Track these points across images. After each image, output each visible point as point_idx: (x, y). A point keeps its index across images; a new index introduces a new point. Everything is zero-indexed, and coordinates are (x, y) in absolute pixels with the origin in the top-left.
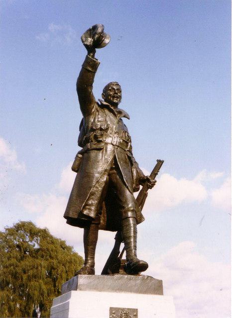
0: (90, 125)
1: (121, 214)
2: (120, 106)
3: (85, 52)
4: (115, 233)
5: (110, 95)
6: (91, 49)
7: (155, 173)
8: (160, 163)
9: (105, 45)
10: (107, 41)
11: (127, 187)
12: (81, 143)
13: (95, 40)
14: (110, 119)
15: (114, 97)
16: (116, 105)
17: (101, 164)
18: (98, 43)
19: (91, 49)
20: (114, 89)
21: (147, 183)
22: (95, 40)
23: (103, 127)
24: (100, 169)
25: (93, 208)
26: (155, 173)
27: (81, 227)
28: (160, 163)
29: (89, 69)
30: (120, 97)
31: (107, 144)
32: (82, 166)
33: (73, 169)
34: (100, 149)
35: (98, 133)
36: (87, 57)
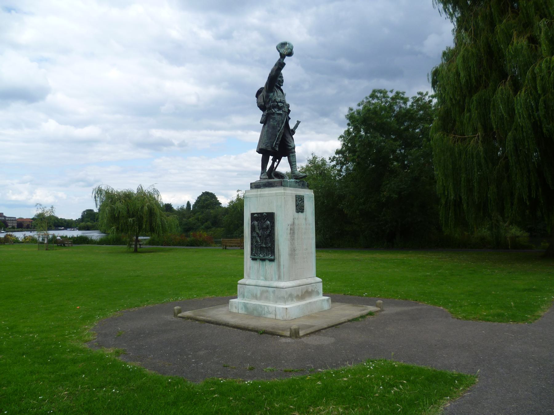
7: (296, 127)
8: (298, 122)
21: (293, 132)
26: (296, 127)
28: (298, 122)
29: (280, 65)
35: (279, 104)
36: (279, 60)
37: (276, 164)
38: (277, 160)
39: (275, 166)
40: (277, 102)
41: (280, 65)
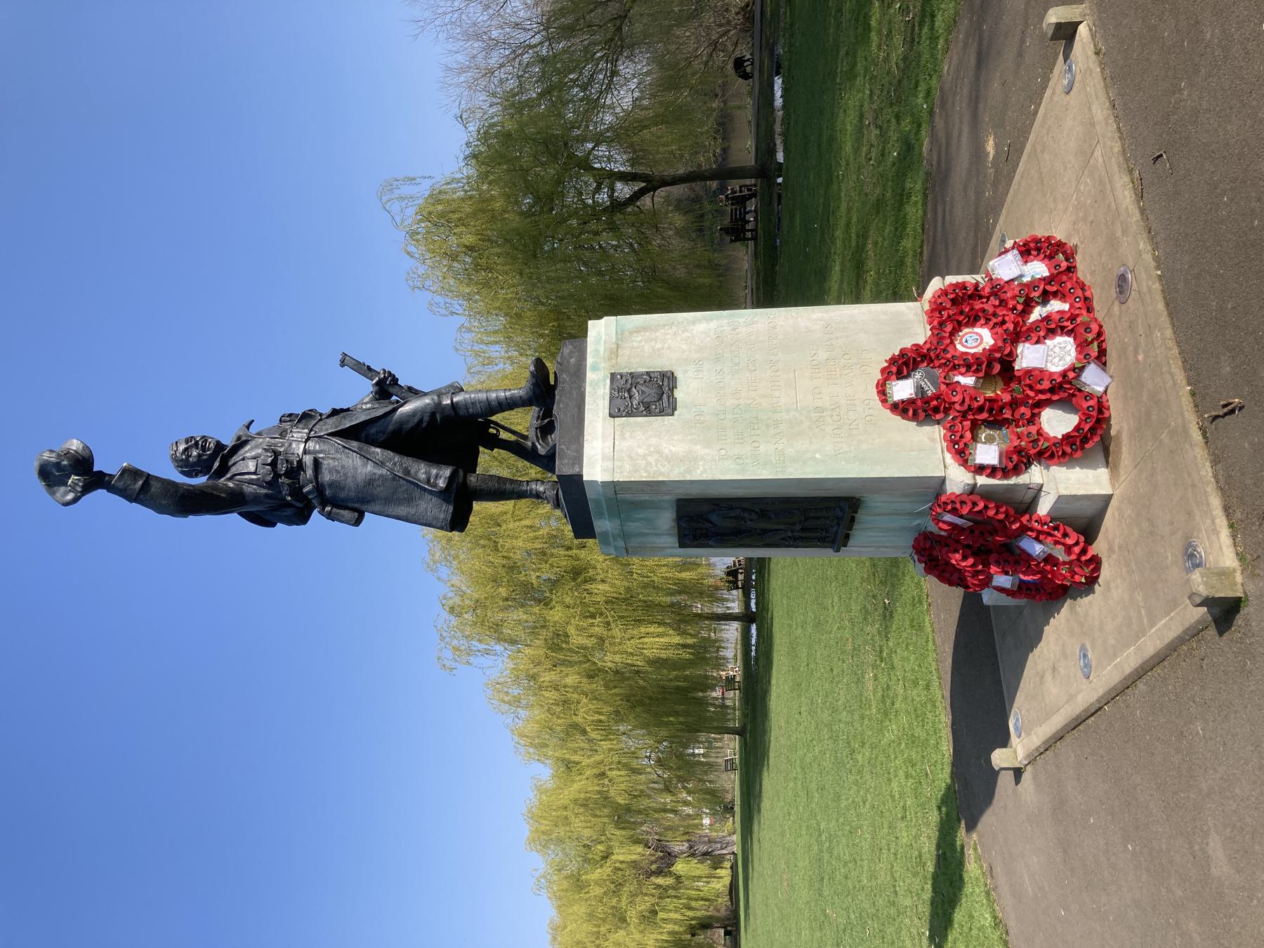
0: (264, 491)
1: (446, 419)
2: (229, 441)
3: (101, 494)
4: (481, 449)
5: (199, 455)
6: (95, 480)
7: (368, 371)
9: (86, 447)
10: (75, 445)
11: (395, 410)
12: (301, 517)
13: (78, 473)
14: (252, 449)
15: (204, 449)
16: (219, 446)
17: (352, 465)
18: (82, 464)
19: (95, 480)
20: (186, 449)
21: (386, 387)
22: (78, 473)
23: (269, 460)
24: (358, 461)
25: (434, 472)
26: (368, 371)
27: (469, 510)
29: (139, 488)
30: (205, 439)
31: (305, 452)
32: (349, 505)
33: (357, 522)
34: (317, 463)
35: (282, 468)
37: (504, 435)
38: (492, 431)
39: (513, 438)
40: (277, 476)
41: (139, 488)
